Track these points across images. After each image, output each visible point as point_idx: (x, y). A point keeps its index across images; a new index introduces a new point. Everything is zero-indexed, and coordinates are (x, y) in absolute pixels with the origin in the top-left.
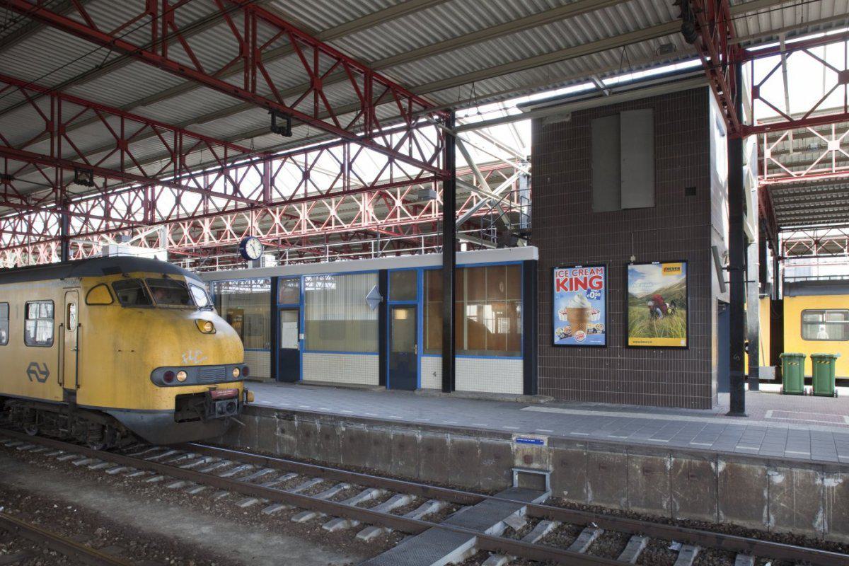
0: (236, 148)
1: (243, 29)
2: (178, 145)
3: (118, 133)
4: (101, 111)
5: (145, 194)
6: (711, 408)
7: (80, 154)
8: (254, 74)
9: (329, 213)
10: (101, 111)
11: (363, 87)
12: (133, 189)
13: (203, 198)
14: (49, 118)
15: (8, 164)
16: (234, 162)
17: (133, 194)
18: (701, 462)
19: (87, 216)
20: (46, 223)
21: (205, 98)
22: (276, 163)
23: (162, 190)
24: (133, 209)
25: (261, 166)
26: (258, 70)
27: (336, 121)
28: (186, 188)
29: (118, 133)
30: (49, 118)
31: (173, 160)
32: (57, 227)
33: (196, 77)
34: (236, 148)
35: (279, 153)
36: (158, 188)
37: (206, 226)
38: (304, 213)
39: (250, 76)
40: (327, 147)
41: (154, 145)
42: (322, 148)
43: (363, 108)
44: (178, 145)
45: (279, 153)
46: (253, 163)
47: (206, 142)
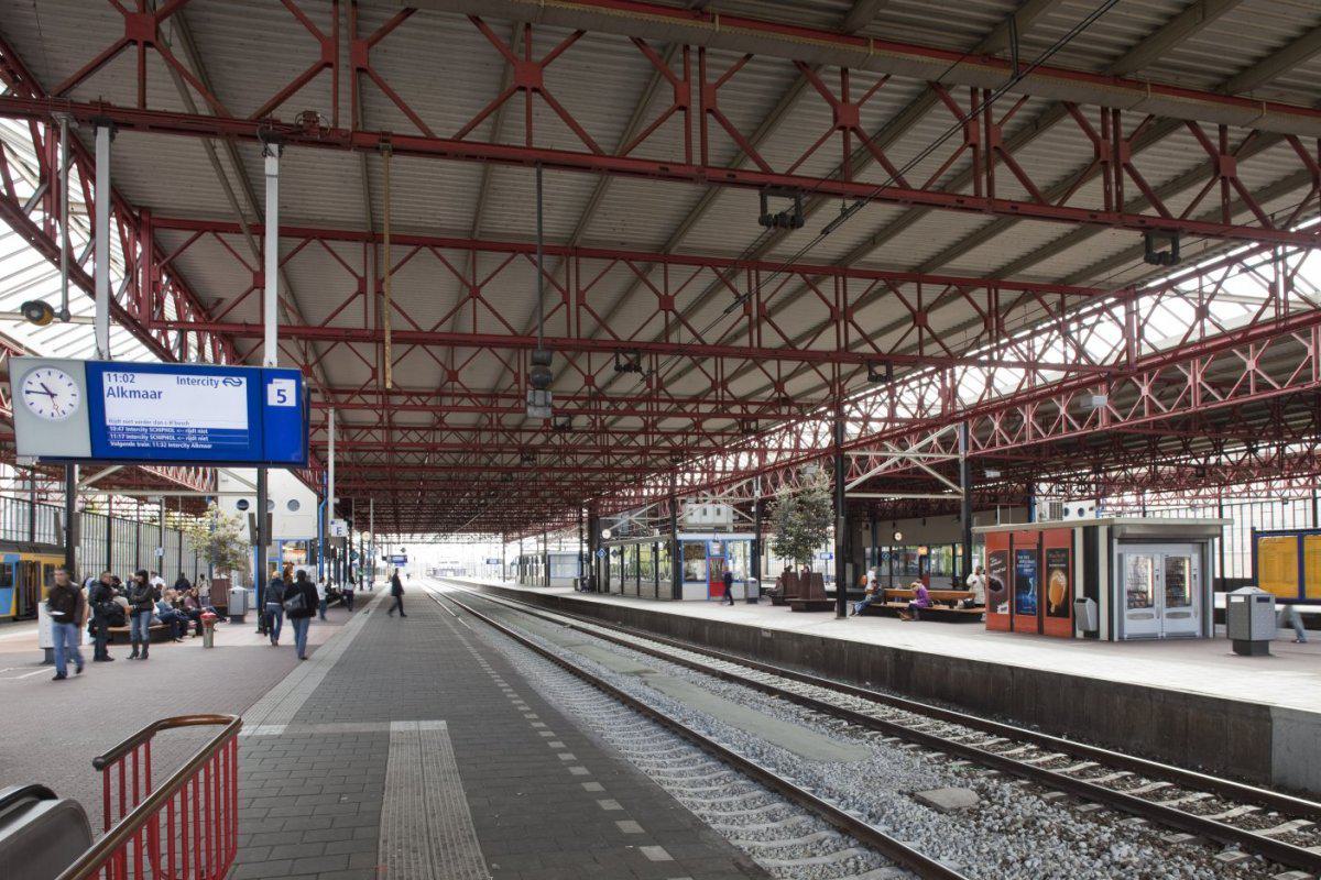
0: (1071, 294)
1: (1099, 125)
2: (993, 305)
3: (915, 307)
4: (811, 274)
5: (943, 379)
6: (1168, 560)
7: (867, 339)
8: (1119, 181)
9: (1243, 366)
10: (890, 280)
11: (71, 183)
12: (925, 375)
13: (1027, 374)
14: (834, 304)
15: (782, 367)
16: (1078, 310)
17: (925, 380)
18: (771, 554)
19: (867, 418)
20: (816, 434)
21: (1028, 234)
22: (1145, 303)
23: (965, 371)
24: (927, 403)
25: (1120, 311)
26: (1126, 175)
27: (1160, 208)
28: (1000, 363)
29: (915, 307)
30: (834, 304)
31: (761, 306)
32: (829, 437)
33: (919, 203)
34: (1079, 292)
35: (1151, 285)
36: (959, 370)
37: (1028, 418)
38: (1194, 376)
39: (1114, 187)
40: (1238, 259)
41: (959, 310)
42: (1230, 262)
43: (1217, 170)
44: (993, 305)
45: (1151, 285)
46: (1107, 308)
47: (1032, 291)
